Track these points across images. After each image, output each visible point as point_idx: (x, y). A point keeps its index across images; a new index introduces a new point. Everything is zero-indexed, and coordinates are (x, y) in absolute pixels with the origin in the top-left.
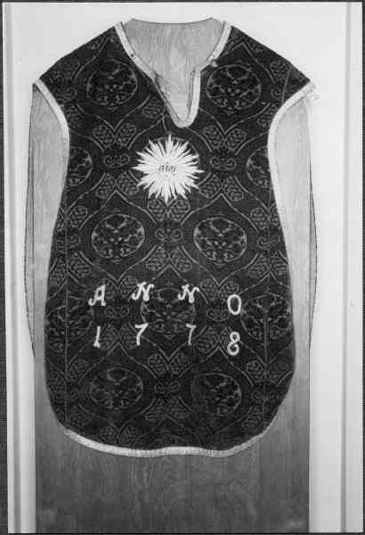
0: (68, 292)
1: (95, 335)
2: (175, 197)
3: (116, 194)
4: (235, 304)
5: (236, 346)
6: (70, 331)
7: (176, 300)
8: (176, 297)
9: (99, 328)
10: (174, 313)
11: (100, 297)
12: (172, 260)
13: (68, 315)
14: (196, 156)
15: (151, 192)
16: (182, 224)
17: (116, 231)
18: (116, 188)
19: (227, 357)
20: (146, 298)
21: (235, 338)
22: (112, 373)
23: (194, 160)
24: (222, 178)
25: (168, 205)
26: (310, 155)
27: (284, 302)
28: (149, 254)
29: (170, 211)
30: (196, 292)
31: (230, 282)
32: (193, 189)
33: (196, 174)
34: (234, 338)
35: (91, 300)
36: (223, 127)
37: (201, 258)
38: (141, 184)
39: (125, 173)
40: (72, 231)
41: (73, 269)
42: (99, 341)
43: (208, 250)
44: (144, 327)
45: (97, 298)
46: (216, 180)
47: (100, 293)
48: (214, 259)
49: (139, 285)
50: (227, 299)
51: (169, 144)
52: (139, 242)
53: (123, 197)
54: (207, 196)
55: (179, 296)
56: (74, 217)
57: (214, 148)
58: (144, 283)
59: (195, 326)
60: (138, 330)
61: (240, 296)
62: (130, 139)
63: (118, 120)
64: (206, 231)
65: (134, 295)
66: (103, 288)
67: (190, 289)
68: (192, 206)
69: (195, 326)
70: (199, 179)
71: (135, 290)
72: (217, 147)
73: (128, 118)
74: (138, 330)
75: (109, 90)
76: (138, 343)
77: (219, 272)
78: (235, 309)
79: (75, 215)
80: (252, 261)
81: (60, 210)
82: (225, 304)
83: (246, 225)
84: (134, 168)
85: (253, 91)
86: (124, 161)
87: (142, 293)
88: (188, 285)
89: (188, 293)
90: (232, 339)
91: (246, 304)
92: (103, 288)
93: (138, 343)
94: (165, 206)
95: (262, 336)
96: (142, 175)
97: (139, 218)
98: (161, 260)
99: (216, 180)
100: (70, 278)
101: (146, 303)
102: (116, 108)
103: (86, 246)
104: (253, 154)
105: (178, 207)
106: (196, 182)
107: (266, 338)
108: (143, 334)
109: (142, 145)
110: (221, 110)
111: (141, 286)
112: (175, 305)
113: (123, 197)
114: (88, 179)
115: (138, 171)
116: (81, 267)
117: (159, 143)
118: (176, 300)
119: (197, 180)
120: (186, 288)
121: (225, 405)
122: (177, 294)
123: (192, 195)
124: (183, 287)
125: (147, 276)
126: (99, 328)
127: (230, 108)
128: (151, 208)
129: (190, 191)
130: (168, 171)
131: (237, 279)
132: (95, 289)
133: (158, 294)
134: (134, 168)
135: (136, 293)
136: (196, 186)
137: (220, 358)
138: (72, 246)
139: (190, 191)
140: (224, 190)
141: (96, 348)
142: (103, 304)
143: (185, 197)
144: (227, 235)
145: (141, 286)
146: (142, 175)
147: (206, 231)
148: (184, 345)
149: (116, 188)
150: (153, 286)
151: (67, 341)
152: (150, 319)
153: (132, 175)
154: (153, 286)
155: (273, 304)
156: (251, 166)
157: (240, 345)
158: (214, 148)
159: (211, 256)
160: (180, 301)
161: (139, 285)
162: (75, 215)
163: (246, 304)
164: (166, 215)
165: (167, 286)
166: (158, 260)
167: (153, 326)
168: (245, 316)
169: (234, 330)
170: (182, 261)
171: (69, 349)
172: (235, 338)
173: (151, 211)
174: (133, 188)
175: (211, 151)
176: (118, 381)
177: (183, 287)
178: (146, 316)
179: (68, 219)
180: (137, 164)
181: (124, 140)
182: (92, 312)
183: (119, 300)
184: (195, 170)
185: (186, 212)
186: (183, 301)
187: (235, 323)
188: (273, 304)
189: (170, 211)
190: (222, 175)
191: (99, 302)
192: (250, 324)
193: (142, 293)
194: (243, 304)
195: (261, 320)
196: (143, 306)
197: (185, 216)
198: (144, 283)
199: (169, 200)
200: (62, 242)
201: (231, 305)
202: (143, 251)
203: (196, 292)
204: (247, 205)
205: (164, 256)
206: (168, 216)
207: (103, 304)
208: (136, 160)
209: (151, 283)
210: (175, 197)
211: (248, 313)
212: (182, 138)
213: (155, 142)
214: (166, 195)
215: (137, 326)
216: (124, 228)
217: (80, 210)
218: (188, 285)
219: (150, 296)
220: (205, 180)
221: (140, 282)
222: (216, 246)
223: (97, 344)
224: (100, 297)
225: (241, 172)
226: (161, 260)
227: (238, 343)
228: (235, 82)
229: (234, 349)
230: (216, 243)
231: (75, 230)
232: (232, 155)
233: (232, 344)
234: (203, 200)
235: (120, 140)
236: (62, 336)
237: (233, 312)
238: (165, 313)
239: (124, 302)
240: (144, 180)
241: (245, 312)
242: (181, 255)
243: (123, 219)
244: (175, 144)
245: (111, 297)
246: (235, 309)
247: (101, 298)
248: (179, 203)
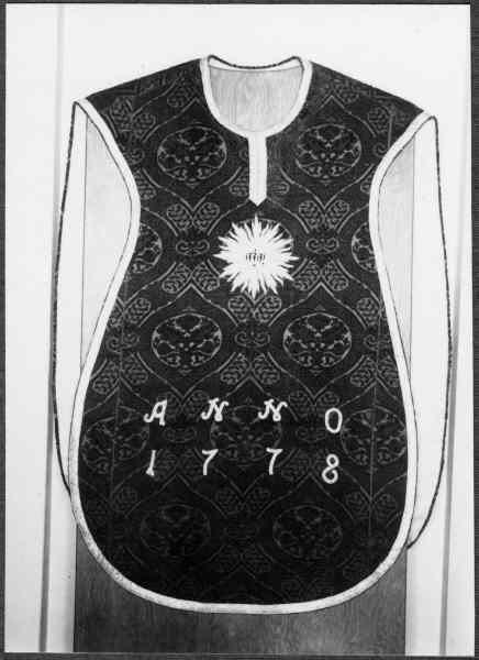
0: (119, 400)
1: (149, 460)
2: (265, 291)
3: (191, 288)
4: (334, 420)
5: (334, 472)
6: (118, 448)
7: (256, 420)
8: (256, 416)
9: (154, 452)
10: (251, 437)
11: (158, 413)
12: (253, 370)
13: (117, 429)
14: (290, 241)
15: (236, 285)
16: (209, 234)
17: (187, 335)
18: (192, 281)
19: (321, 487)
20: (219, 418)
21: (333, 461)
22: (169, 512)
23: (287, 246)
24: (321, 264)
25: (255, 303)
26: (414, 224)
27: (397, 422)
28: (226, 364)
29: (257, 310)
30: (283, 407)
31: (329, 393)
32: (286, 281)
33: (291, 262)
34: (332, 463)
35: (147, 415)
36: (322, 200)
37: (289, 365)
38: (222, 276)
39: (203, 263)
40: (128, 328)
41: (127, 372)
42: (154, 469)
43: (302, 355)
44: (213, 453)
45: (155, 414)
46: (313, 267)
47: (160, 409)
48: (310, 364)
49: (210, 402)
50: (324, 413)
51: (257, 225)
52: (214, 349)
53: (199, 293)
54: (302, 289)
55: (260, 414)
56: (133, 311)
57: (312, 227)
58: (217, 400)
59: (280, 451)
60: (206, 457)
61: (341, 410)
62: (146, 131)
63: (199, 199)
64: (300, 331)
65: (203, 414)
66: (164, 404)
67: (275, 405)
68: (284, 302)
69: (280, 451)
70: (294, 268)
71: (206, 407)
72: (316, 226)
73: (358, 393)
74: (206, 457)
75: (188, 163)
76: (205, 473)
77: (316, 383)
78: (334, 426)
79: (135, 309)
80: (357, 364)
81: (117, 301)
82: (323, 420)
83: (350, 319)
84: (216, 256)
85: (351, 151)
86: (202, 249)
87: (214, 412)
88: (272, 401)
89: (273, 410)
90: (329, 463)
91: (348, 420)
92: (164, 404)
93: (205, 473)
94: (252, 303)
95: (368, 461)
96: (225, 264)
97: (216, 320)
98: (241, 371)
99: (313, 267)
100: (123, 384)
101: (218, 423)
102: (197, 184)
103: (146, 348)
104: (359, 230)
105: (268, 305)
106: (290, 271)
107: (372, 463)
108: (212, 461)
109: (225, 229)
110: (315, 181)
111: (213, 403)
112: (253, 427)
113: (199, 293)
114: (156, 267)
115: (218, 259)
116: (137, 371)
117: (246, 226)
118: (256, 420)
119: (290, 269)
120: (269, 404)
121: (259, 446)
122: (258, 411)
123: (285, 289)
124: (266, 403)
125: (220, 391)
126: (154, 452)
127: (326, 177)
128: (232, 306)
129: (282, 282)
130: (256, 259)
131: (335, 388)
132: (155, 402)
133: (296, 512)
134: (216, 256)
135: (207, 412)
136: (290, 278)
137: (314, 486)
138: (129, 346)
139: (282, 282)
140: (324, 277)
141: (149, 476)
142: (162, 423)
143: (275, 292)
144: (326, 334)
145: (213, 403)
146: (225, 264)
147: (300, 331)
148: (262, 476)
149: (310, 470)
150: (227, 404)
151: (114, 460)
152: (220, 445)
153: (212, 266)
154: (227, 404)
155: (384, 421)
156: (357, 245)
157: (339, 472)
158: (312, 227)
159: (181, 176)
160: (262, 421)
161: (210, 402)
162: (135, 309)
163: (348, 420)
164: (251, 315)
165: (246, 399)
166: (234, 371)
167: (223, 452)
168: (346, 435)
169: (331, 453)
170: (265, 370)
171: (115, 469)
172: (333, 461)
173: (232, 310)
174: (212, 282)
175: (307, 232)
176: (177, 520)
177: (266, 403)
178: (216, 441)
179: (127, 312)
180: (219, 251)
181: (141, 131)
182: (147, 430)
183: (185, 421)
184: (289, 257)
185: (277, 310)
186: (265, 420)
187: (332, 444)
188: (384, 421)
189: (257, 310)
190: (322, 261)
191: (157, 420)
192: (352, 446)
193: (214, 412)
194: (344, 419)
195: (368, 440)
196: (214, 428)
197: (275, 316)
198: (217, 400)
199: (257, 295)
200: (117, 340)
201: (330, 421)
202: (218, 360)
203: (283, 407)
204: (351, 296)
205: (244, 365)
206: (254, 316)
207: (162, 423)
208: (217, 246)
209: (225, 400)
210: (265, 291)
211: (351, 432)
212: (271, 218)
213: (241, 226)
214: (254, 289)
215: (204, 452)
216: (197, 331)
217: (141, 302)
218: (272, 401)
219: (224, 415)
220: (300, 268)
221: (212, 398)
222: (313, 349)
223: (150, 472)
224: (158, 413)
225: (344, 255)
226: (241, 371)
227: (336, 469)
228: (329, 145)
229: (330, 476)
230: (313, 345)
231: (133, 327)
232: (333, 233)
233: (328, 469)
234: (299, 294)
235: (198, 223)
236: (107, 454)
237: (329, 428)
238: (239, 437)
239: (192, 422)
240: (227, 271)
241: (346, 430)
242: (267, 364)
243: (198, 320)
244: (263, 226)
245: (173, 416)
246: (334, 426)
247: (161, 416)
248: (269, 300)
